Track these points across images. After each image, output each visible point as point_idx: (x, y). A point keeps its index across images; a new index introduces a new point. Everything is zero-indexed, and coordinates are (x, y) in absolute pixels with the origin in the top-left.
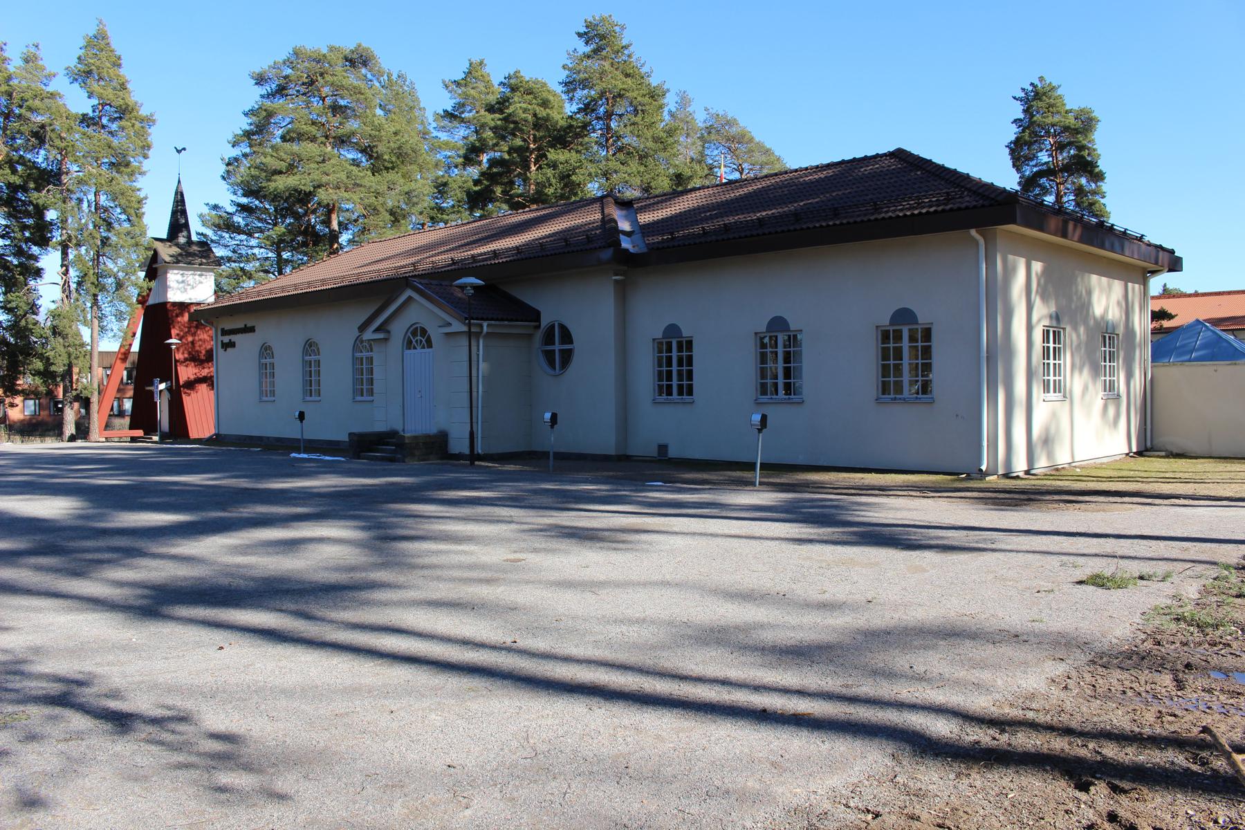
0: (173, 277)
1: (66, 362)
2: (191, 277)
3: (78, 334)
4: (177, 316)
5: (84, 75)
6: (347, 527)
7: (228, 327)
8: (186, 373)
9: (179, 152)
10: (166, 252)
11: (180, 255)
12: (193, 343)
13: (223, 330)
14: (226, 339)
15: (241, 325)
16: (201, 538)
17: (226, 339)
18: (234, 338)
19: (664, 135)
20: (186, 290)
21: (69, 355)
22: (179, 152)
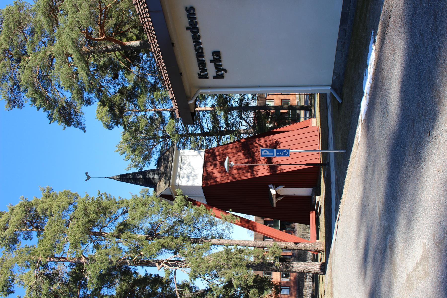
0: (182, 182)
1: (244, 269)
2: (184, 171)
3: (217, 255)
4: (216, 181)
5: (46, 258)
6: (408, 240)
7: (196, 70)
8: (262, 170)
9: (89, 178)
10: (162, 187)
11: (165, 178)
12: (238, 169)
13: (201, 77)
14: (211, 69)
15: (189, 34)
16: (434, 133)
17: (211, 69)
18: (208, 57)
19: (216, 98)
20: (195, 175)
21: (236, 265)
22: (89, 178)
